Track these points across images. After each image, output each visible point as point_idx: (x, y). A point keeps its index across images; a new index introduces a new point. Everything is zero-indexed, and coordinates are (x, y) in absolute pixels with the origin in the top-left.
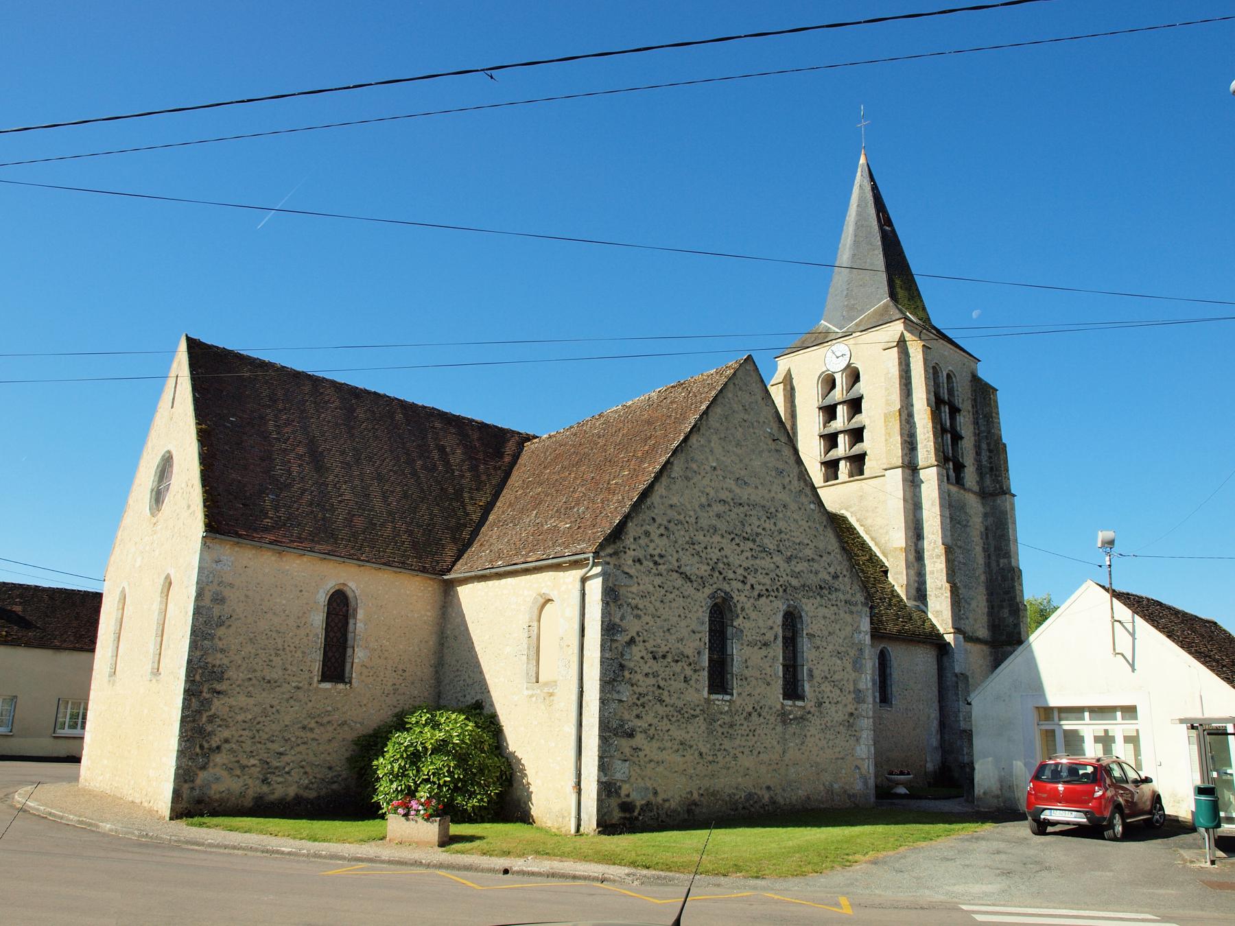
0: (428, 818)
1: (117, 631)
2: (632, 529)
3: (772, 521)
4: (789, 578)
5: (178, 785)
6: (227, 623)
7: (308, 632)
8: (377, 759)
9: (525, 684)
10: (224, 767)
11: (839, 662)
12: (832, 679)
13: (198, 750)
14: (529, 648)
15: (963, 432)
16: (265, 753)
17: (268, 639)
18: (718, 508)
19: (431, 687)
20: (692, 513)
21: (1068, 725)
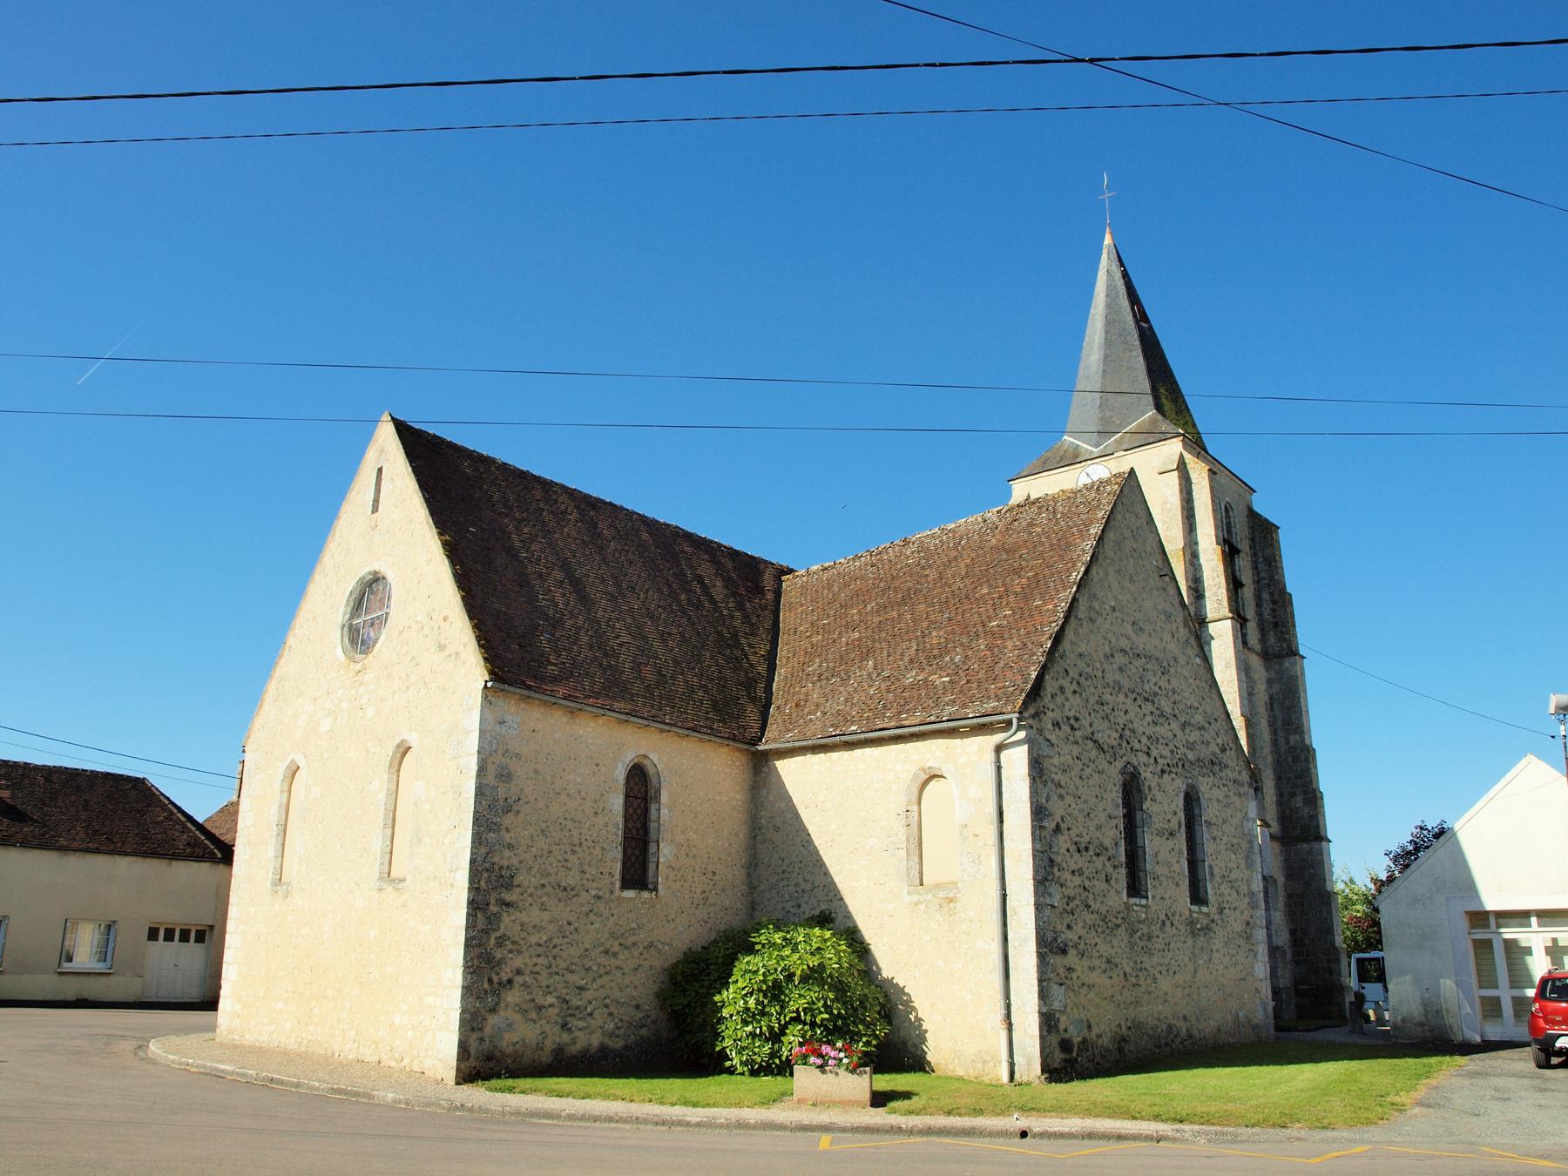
0: (853, 1070)
1: (283, 822)
2: (1050, 685)
3: (1167, 677)
4: (1185, 750)
5: (465, 1035)
6: (515, 808)
7: (607, 821)
8: (720, 993)
9: (906, 887)
10: (518, 1008)
11: (1233, 856)
12: (1230, 879)
13: (486, 985)
14: (908, 840)
15: (1243, 578)
16: (563, 987)
17: (562, 829)
18: (1120, 659)
19: (743, 895)
20: (1098, 665)
21: (1508, 933)
